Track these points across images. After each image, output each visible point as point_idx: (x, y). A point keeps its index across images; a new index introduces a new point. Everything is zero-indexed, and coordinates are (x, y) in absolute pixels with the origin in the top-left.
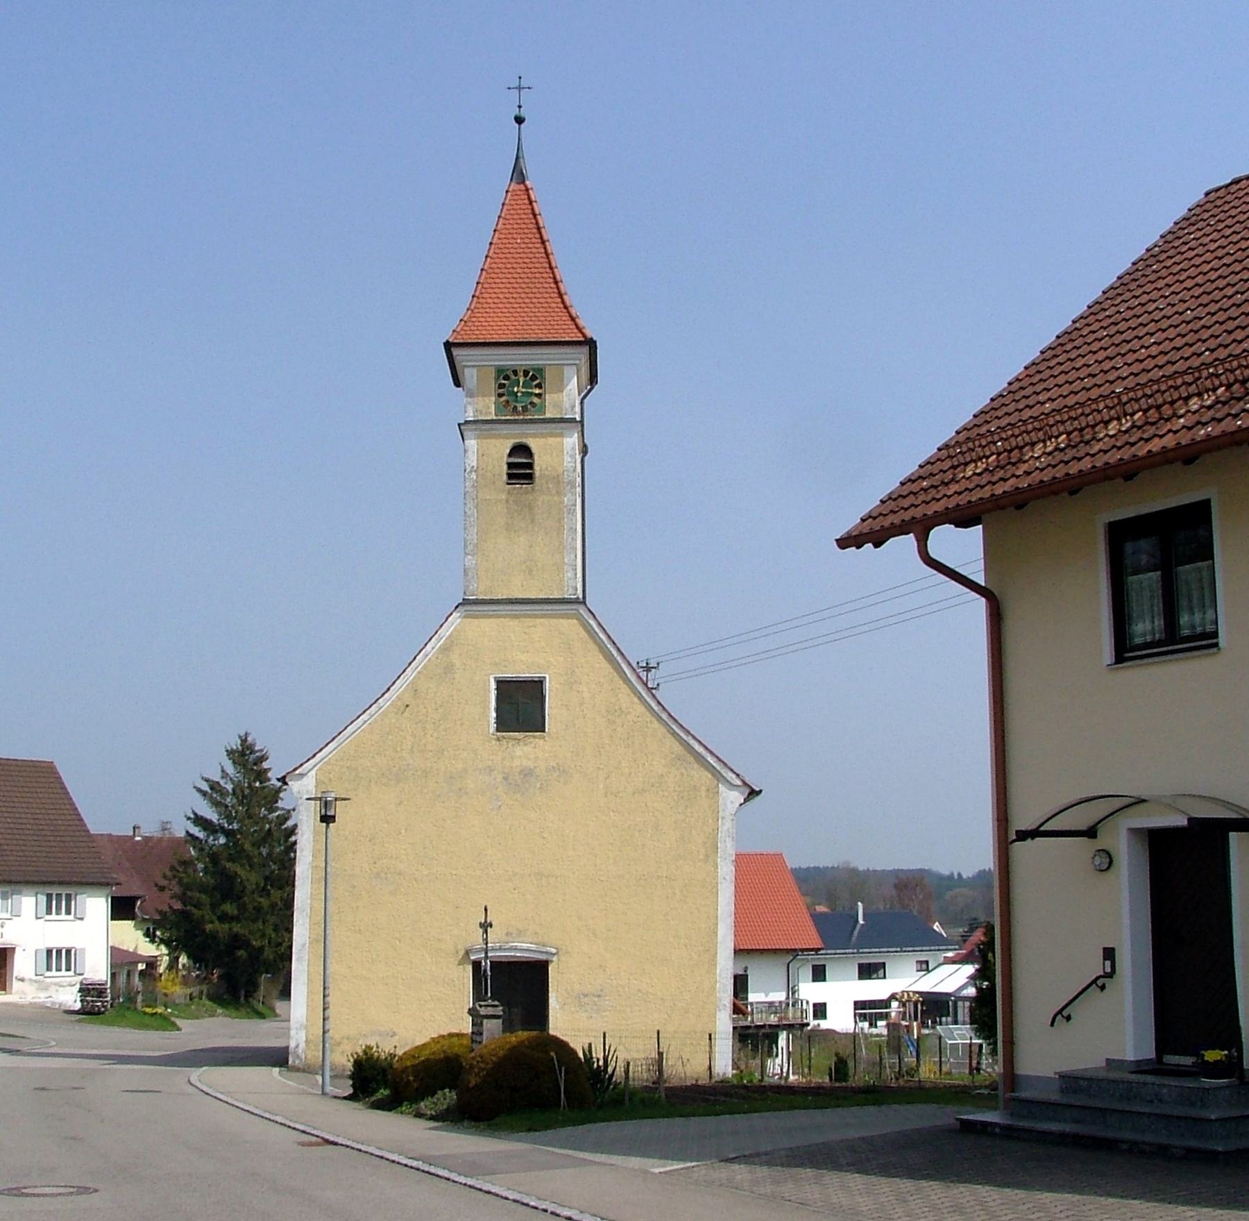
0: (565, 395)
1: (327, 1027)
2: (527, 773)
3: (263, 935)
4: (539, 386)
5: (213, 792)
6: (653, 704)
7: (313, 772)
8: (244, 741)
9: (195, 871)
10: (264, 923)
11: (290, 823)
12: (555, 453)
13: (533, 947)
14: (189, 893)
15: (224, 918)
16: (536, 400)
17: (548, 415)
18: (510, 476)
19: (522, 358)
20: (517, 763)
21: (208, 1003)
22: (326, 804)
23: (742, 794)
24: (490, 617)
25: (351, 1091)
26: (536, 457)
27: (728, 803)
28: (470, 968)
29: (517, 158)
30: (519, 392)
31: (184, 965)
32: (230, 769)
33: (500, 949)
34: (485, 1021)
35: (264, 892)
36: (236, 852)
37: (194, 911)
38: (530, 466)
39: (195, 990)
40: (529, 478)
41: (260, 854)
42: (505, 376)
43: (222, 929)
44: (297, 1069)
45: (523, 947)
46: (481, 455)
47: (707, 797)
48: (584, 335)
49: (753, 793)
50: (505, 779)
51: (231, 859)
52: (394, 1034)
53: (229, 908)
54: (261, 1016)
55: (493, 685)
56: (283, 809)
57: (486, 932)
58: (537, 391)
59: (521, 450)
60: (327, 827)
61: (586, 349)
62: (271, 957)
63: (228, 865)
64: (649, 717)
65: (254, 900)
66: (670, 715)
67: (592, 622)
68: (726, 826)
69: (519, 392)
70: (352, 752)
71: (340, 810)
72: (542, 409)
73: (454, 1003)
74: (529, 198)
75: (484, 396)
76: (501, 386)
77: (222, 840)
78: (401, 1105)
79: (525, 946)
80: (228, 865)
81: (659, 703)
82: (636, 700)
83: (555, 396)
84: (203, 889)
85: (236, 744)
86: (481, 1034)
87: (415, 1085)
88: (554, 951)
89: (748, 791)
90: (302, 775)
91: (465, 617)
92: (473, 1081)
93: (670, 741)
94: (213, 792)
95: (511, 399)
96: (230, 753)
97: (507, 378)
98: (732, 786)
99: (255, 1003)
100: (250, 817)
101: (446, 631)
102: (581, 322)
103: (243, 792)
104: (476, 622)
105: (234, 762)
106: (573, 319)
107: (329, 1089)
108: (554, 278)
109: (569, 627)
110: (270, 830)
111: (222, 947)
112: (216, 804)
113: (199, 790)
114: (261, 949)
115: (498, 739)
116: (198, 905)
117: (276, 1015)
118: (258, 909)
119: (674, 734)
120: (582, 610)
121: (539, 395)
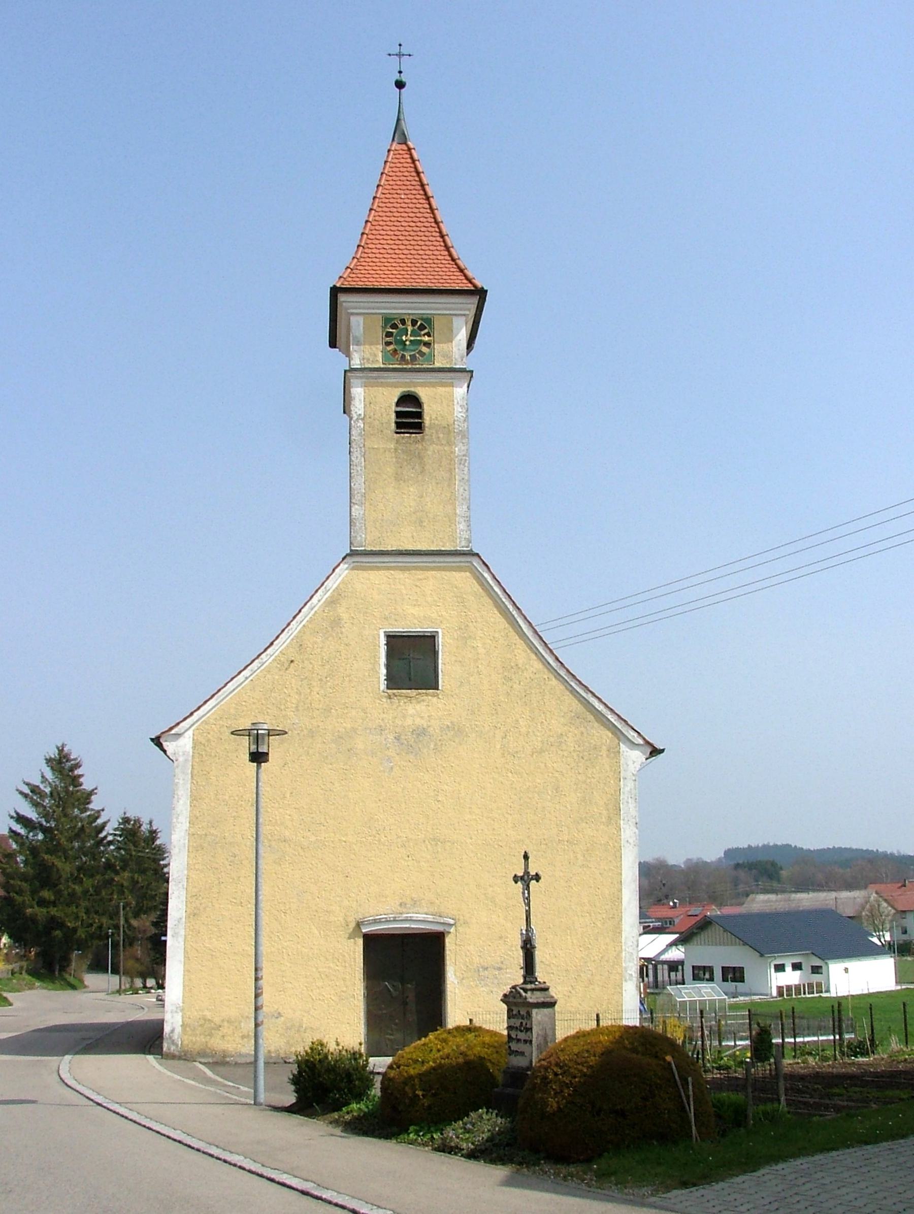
0: (451, 348)
1: (260, 1019)
2: (421, 732)
3: (77, 918)
4: (429, 335)
5: (33, 794)
6: (551, 660)
7: (190, 732)
8: (61, 751)
9: (17, 863)
10: (77, 907)
11: (99, 821)
12: (442, 402)
13: (430, 918)
14: (12, 882)
15: (42, 903)
16: (424, 349)
17: (437, 365)
18: (399, 425)
19: (405, 309)
20: (409, 721)
21: (27, 977)
22: (258, 739)
23: (644, 753)
24: (378, 569)
25: (290, 1098)
26: (425, 407)
27: (630, 763)
28: (360, 941)
29: (398, 120)
30: (407, 341)
31: (5, 944)
32: (49, 775)
33: (395, 920)
34: (534, 1011)
35: (77, 880)
36: (52, 844)
37: (17, 897)
38: (419, 415)
39: (16, 966)
40: (418, 427)
41: (73, 848)
42: (392, 327)
43: (40, 912)
44: (173, 1057)
45: (418, 918)
46: (368, 404)
47: (608, 756)
48: (475, 286)
49: (655, 752)
50: (397, 738)
51: (49, 852)
52: (280, 1015)
53: (46, 894)
54: (74, 987)
55: (383, 641)
56: (92, 810)
57: (528, 887)
58: (426, 338)
59: (409, 399)
60: (258, 768)
61: (475, 300)
62: (83, 936)
63: (46, 857)
64: (546, 674)
65: (68, 887)
66: (568, 671)
67: (486, 575)
68: (627, 787)
69: (407, 341)
70: (232, 711)
71: (275, 748)
72: (431, 358)
73: (344, 979)
74: (412, 158)
75: (371, 344)
76: (389, 335)
77: (40, 837)
78: (406, 1131)
79: (421, 917)
80: (46, 857)
81: (557, 659)
82: (533, 656)
83: (444, 346)
84: (24, 878)
85: (53, 753)
86: (529, 1029)
87: (426, 1102)
88: (452, 922)
89: (649, 750)
90: (178, 735)
91: (353, 569)
92: (553, 1103)
93: (569, 698)
94: (33, 794)
95: (398, 347)
96: (49, 761)
97: (394, 326)
98: (633, 745)
99: (67, 976)
100: (66, 815)
101: (332, 584)
102: (470, 274)
103: (59, 794)
104: (365, 574)
105: (52, 768)
106: (461, 271)
107: (262, 1098)
108: (440, 232)
109: (462, 580)
110: (83, 826)
111: (40, 928)
112: (36, 805)
113: (21, 793)
114: (75, 930)
115: (389, 697)
116: (20, 892)
117: (85, 987)
118: (73, 895)
119: (573, 691)
120: (476, 562)
121: (427, 344)
